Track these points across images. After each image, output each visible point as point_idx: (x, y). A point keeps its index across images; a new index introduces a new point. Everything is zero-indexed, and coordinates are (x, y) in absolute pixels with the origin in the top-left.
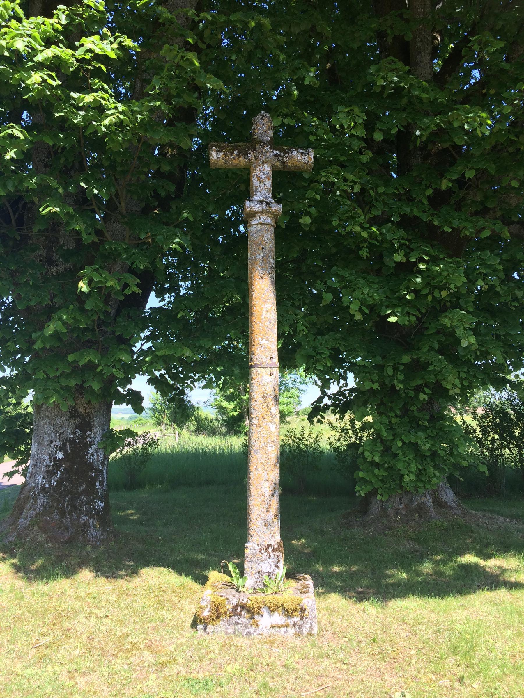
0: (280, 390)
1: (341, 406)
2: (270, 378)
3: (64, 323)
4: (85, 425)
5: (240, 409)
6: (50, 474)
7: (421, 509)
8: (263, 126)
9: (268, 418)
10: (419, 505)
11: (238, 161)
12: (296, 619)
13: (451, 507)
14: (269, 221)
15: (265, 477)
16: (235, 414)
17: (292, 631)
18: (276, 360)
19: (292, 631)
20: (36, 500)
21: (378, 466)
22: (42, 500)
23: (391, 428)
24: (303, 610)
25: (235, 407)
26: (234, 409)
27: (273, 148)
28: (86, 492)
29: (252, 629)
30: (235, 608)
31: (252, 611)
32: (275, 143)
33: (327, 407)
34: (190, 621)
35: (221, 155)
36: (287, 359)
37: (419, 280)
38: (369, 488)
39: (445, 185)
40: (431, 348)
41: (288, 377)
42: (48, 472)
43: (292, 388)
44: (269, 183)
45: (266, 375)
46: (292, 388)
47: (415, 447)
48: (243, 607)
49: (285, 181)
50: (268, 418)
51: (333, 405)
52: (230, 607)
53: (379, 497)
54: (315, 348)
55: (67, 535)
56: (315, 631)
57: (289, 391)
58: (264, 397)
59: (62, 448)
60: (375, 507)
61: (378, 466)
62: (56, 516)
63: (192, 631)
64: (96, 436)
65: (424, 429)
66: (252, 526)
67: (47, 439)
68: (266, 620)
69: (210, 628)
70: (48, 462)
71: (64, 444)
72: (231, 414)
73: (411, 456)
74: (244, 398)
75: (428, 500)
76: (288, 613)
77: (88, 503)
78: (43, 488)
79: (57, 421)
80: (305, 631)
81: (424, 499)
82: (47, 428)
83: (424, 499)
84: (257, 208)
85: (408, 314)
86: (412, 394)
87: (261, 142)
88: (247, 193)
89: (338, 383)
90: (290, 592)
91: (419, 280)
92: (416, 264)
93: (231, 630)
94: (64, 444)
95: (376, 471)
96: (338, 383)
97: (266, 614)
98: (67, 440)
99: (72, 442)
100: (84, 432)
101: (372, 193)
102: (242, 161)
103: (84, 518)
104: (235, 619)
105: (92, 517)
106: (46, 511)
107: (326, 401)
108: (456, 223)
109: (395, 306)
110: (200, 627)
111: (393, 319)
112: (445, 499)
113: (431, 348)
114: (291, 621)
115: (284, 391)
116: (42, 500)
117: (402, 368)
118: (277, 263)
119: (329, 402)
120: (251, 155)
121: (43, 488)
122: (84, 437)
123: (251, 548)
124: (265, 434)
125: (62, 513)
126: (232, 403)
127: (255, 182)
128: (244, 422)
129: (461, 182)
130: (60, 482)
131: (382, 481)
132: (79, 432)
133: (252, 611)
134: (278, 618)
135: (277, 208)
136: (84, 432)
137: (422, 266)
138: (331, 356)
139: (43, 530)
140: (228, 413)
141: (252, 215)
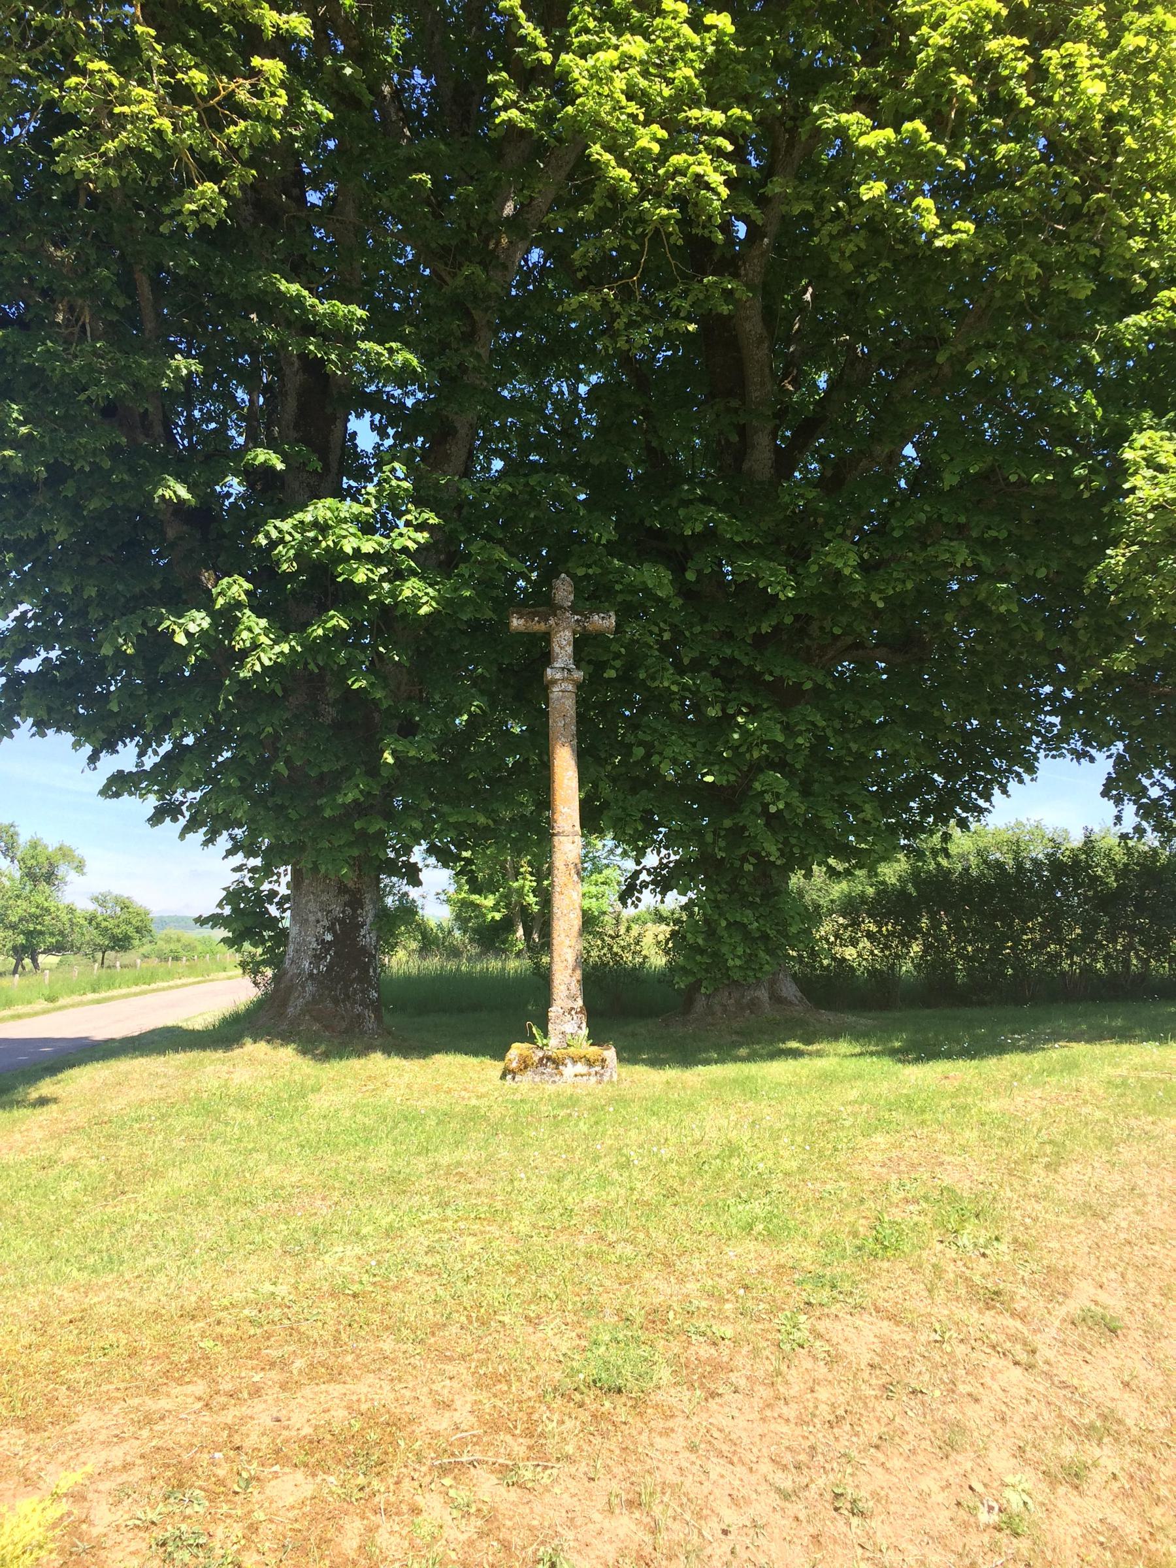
0: (584, 869)
1: (664, 882)
2: (571, 847)
3: (361, 792)
4: (355, 902)
5: (507, 907)
6: (317, 958)
7: (754, 1005)
8: (564, 591)
9: (570, 886)
10: (752, 1000)
11: (538, 627)
12: (598, 1069)
13: (791, 1003)
14: (570, 687)
15: (567, 943)
16: (498, 916)
17: (593, 1079)
18: (578, 828)
19: (593, 1079)
20: (303, 987)
21: (702, 952)
22: (310, 988)
23: (718, 907)
24: (604, 1061)
25: (497, 904)
26: (495, 908)
27: (575, 613)
28: (359, 980)
29: (557, 1078)
30: (541, 1059)
31: (557, 1062)
32: (574, 609)
33: (645, 885)
34: (499, 1074)
35: (522, 622)
36: (591, 820)
37: (736, 736)
38: (691, 979)
39: (765, 628)
40: (753, 812)
41: (599, 845)
42: (315, 956)
43: (607, 866)
44: (570, 649)
45: (568, 845)
46: (607, 866)
47: (741, 927)
48: (549, 1058)
49: (583, 644)
50: (570, 886)
51: (653, 882)
52: (536, 1059)
53: (703, 990)
54: (624, 809)
55: (344, 1025)
56: (615, 1078)
57: (600, 872)
58: (567, 865)
59: (330, 929)
60: (700, 1004)
61: (702, 952)
62: (330, 1004)
63: (499, 1082)
64: (368, 914)
65: (752, 905)
66: (555, 991)
67: (312, 918)
68: (569, 1070)
69: (518, 1078)
70: (315, 945)
71: (333, 924)
72: (489, 917)
73: (738, 938)
74: (516, 885)
75: (763, 994)
76: (590, 1063)
77: (362, 991)
78: (311, 974)
79: (325, 897)
80: (606, 1078)
81: (758, 993)
82: (312, 906)
83: (758, 993)
84: (558, 676)
85: (727, 773)
86: (737, 864)
87: (561, 607)
88: (547, 658)
89: (659, 853)
90: (593, 1051)
91: (736, 736)
92: (734, 717)
93: (537, 1079)
94: (333, 924)
95: (698, 958)
96: (659, 853)
97: (570, 1065)
98: (337, 919)
99: (342, 922)
100: (354, 910)
101: (687, 634)
102: (542, 627)
103: (359, 1009)
104: (541, 1069)
105: (367, 1007)
106: (314, 1001)
107: (644, 876)
108: (778, 671)
109: (713, 764)
110: (509, 1077)
111: (709, 779)
112: (784, 994)
113: (753, 812)
114: (593, 1070)
115: (592, 873)
116: (310, 988)
117: (723, 833)
118: (578, 730)
119: (648, 879)
120: (552, 622)
121: (311, 974)
122: (354, 916)
123: (554, 1011)
124: (567, 901)
125: (336, 1001)
126: (491, 897)
127: (557, 649)
128: (515, 932)
129: (777, 629)
130: (330, 968)
131: (706, 971)
132: (349, 910)
133: (557, 1062)
134: (581, 1068)
135: (579, 675)
136: (354, 910)
137: (740, 719)
138: (642, 819)
139: (316, 1019)
140: (484, 915)
141: (554, 682)
